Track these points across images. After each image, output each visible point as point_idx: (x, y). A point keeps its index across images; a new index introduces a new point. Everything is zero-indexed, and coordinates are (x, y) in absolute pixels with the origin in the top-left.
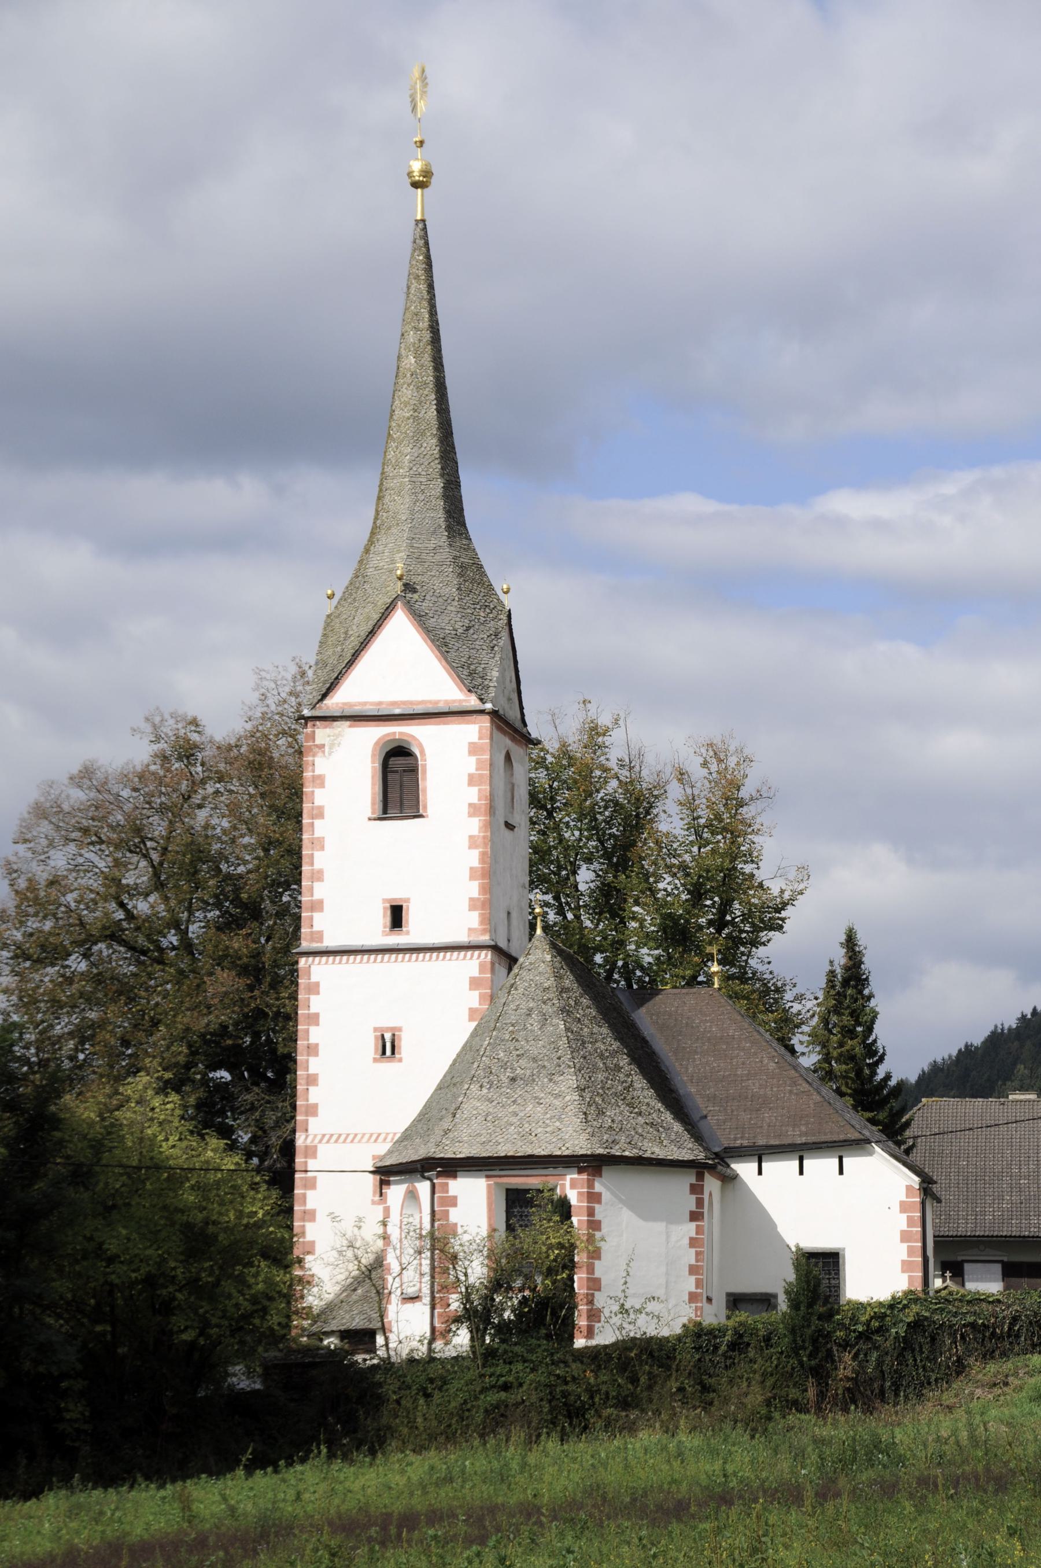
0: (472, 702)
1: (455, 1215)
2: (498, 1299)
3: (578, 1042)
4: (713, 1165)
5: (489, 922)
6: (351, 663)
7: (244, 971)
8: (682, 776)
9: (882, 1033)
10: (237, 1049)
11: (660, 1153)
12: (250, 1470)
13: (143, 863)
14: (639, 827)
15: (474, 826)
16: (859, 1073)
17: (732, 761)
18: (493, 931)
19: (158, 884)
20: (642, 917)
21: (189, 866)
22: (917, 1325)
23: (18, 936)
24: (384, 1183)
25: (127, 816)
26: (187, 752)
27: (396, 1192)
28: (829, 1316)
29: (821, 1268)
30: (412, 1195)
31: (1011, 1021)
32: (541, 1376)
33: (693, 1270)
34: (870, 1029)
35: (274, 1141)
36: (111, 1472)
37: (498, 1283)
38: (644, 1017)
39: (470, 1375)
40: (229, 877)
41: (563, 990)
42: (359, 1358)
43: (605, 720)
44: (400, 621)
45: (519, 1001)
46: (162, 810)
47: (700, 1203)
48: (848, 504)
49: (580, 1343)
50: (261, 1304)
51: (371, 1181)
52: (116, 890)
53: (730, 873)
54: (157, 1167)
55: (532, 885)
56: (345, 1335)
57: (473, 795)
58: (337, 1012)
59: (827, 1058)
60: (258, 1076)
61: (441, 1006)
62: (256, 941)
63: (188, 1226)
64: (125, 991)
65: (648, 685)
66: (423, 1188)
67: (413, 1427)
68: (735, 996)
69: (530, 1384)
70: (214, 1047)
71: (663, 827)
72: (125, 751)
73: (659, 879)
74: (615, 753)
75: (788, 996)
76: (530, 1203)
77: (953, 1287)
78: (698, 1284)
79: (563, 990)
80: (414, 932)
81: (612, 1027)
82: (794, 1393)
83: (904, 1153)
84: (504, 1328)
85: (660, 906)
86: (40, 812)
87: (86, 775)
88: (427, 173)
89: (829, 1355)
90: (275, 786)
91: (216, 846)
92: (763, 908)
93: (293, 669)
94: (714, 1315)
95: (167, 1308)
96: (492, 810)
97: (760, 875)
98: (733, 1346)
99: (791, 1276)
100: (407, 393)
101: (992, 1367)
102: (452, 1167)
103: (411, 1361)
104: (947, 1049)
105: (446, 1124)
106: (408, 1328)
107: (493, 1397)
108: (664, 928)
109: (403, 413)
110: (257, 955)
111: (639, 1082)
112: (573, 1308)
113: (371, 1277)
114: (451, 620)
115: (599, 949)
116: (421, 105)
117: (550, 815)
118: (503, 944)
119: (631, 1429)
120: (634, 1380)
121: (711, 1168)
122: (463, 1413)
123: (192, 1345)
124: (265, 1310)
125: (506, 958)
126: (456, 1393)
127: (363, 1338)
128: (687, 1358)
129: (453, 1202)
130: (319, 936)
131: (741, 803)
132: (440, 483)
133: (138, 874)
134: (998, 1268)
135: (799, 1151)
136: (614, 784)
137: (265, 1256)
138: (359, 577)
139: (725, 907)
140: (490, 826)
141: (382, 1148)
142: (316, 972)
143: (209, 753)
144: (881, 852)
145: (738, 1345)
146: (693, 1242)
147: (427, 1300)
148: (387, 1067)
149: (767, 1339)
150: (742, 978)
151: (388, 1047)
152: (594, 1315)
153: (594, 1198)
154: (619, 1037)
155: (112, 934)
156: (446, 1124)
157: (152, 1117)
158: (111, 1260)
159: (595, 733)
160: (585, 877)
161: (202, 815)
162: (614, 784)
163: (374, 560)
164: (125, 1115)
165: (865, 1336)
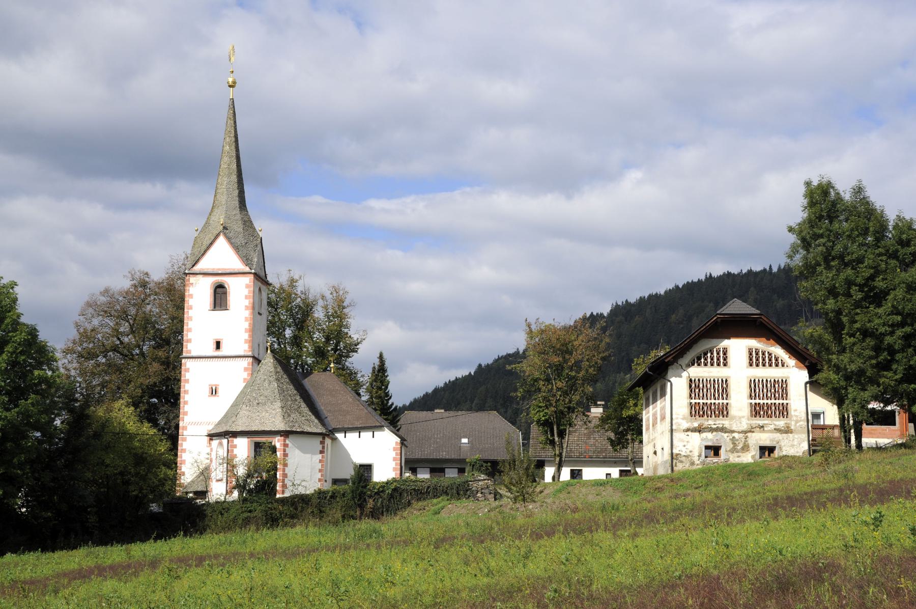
0: (247, 269)
1: (236, 451)
2: (249, 480)
3: (282, 391)
4: (330, 434)
5: (252, 348)
6: (203, 255)
7: (163, 363)
8: (323, 297)
9: (391, 389)
10: (160, 392)
11: (310, 430)
12: (156, 540)
13: (127, 324)
14: (308, 315)
15: (247, 314)
16: (383, 402)
17: (341, 293)
18: (253, 351)
19: (132, 332)
20: (308, 346)
21: (143, 326)
22: (395, 490)
23: (80, 349)
24: (211, 439)
25: (121, 307)
26: (144, 284)
27: (215, 442)
28: (365, 487)
29: (366, 469)
30: (221, 444)
31: (442, 385)
32: (263, 507)
33: (320, 471)
34: (387, 387)
35: (173, 424)
36: (105, 540)
37: (249, 475)
38: (307, 383)
39: (238, 507)
40: (158, 329)
41: (277, 372)
42: (198, 501)
43: (296, 277)
44: (222, 240)
45: (261, 376)
46: (134, 305)
47: (323, 447)
48: (376, 204)
49: (278, 496)
50: (162, 482)
51: (207, 438)
52: (117, 334)
53: (340, 332)
54: (125, 433)
55: (269, 335)
56: (196, 493)
57: (247, 302)
58: (195, 380)
59: (372, 397)
60: (167, 401)
61: (234, 377)
62: (168, 353)
63: (136, 455)
64: (119, 370)
65: (311, 264)
66: (225, 441)
67: (216, 524)
68: (339, 376)
69: (259, 511)
70: (152, 390)
71: (316, 315)
72: (122, 283)
73: (314, 333)
74: (300, 288)
75: (359, 375)
76: (261, 447)
77: (413, 477)
78: (322, 475)
79: (277, 372)
80: (224, 351)
81: (294, 386)
82: (352, 513)
83: (396, 430)
84: (250, 491)
85: (314, 343)
86: (89, 305)
87: (106, 292)
88: (234, 82)
89: (365, 499)
90: (174, 296)
91: (154, 319)
92: (351, 344)
93: (184, 256)
94: (327, 487)
95: (127, 483)
96: (253, 308)
97: (350, 333)
98: (331, 497)
99: (353, 473)
100: (226, 159)
101: (420, 503)
102: (235, 434)
103: (217, 502)
104: (419, 394)
105: (233, 419)
106: (218, 491)
107: (246, 515)
108: (315, 351)
109: (224, 166)
110: (168, 358)
111: (303, 405)
112: (275, 485)
113: (205, 474)
114: (240, 240)
115: (292, 358)
116: (232, 59)
117: (276, 310)
118: (256, 356)
119: (293, 526)
120: (296, 509)
121: (328, 435)
122: (234, 520)
123: (137, 496)
124: (164, 484)
125: (257, 360)
126: (233, 513)
127: (203, 494)
128: (315, 501)
129: (235, 446)
130: (190, 352)
131: (344, 308)
132: (237, 192)
133: (125, 327)
134: (428, 470)
135: (359, 429)
136: (299, 299)
137: (164, 465)
138: (207, 223)
139: (337, 344)
140: (253, 313)
141: (211, 427)
142: (187, 364)
143: (152, 285)
144: (390, 324)
145: (333, 496)
146: (320, 461)
147: (225, 480)
148: (213, 398)
149: (344, 495)
150: (343, 369)
151: (214, 392)
152: (284, 486)
153: (286, 445)
154: (297, 389)
155: (115, 349)
156: (233, 419)
157: (123, 414)
158: (107, 466)
159: (292, 282)
160: (288, 333)
161: (149, 307)
162: (299, 299)
163: (213, 218)
164: (114, 414)
165: (377, 493)
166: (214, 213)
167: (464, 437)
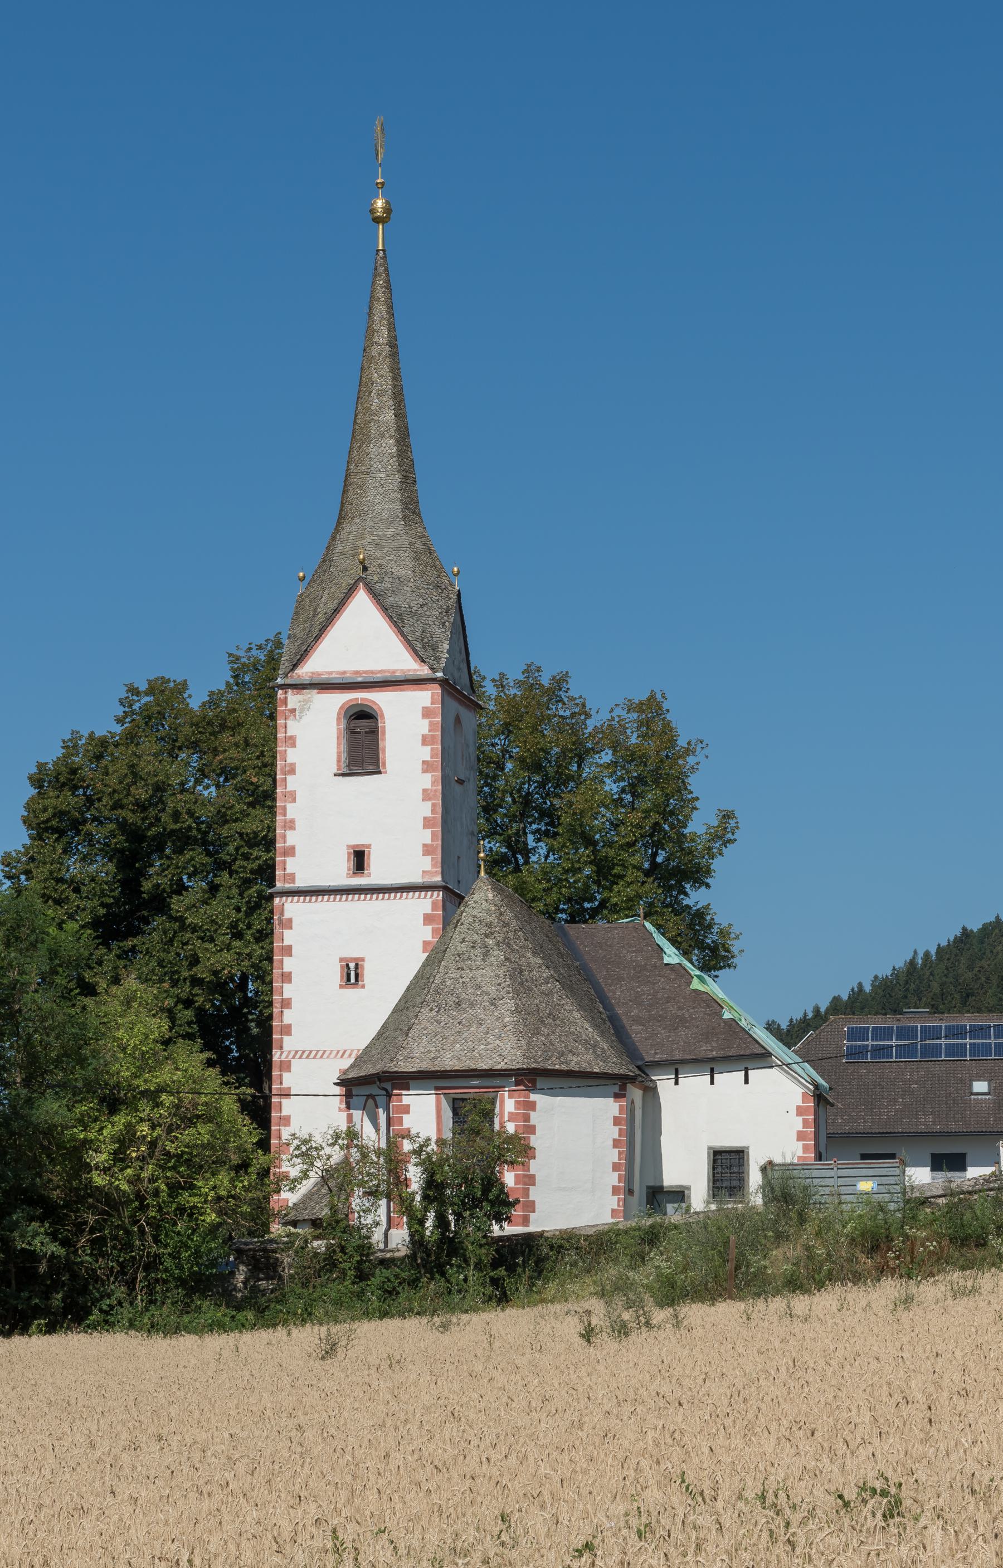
6: (318, 638)
15: (428, 781)
61: (398, 939)
80: (377, 874)
102: (405, 1080)
141: (346, 1063)
151: (352, 975)
166: (343, 535)
167: (979, 1079)
